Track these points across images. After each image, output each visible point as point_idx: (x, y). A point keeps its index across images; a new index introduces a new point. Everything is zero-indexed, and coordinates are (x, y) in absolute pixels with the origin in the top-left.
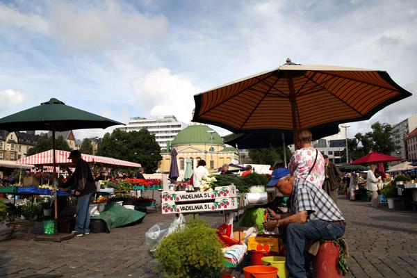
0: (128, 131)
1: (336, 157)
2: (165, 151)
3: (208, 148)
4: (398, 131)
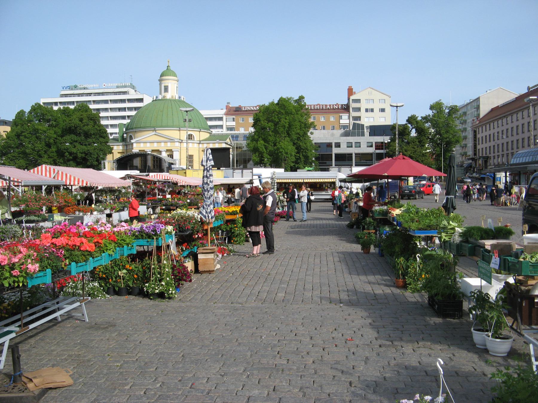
0: (55, 108)
1: (378, 151)
2: (115, 140)
3: (184, 135)
4: (465, 114)
